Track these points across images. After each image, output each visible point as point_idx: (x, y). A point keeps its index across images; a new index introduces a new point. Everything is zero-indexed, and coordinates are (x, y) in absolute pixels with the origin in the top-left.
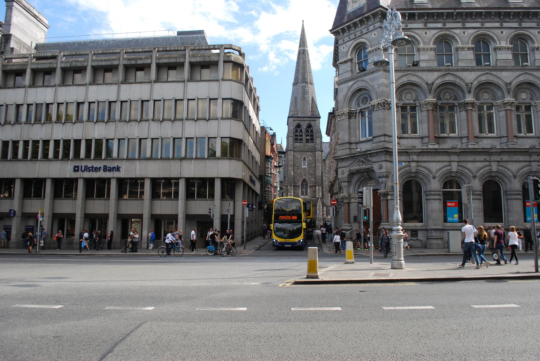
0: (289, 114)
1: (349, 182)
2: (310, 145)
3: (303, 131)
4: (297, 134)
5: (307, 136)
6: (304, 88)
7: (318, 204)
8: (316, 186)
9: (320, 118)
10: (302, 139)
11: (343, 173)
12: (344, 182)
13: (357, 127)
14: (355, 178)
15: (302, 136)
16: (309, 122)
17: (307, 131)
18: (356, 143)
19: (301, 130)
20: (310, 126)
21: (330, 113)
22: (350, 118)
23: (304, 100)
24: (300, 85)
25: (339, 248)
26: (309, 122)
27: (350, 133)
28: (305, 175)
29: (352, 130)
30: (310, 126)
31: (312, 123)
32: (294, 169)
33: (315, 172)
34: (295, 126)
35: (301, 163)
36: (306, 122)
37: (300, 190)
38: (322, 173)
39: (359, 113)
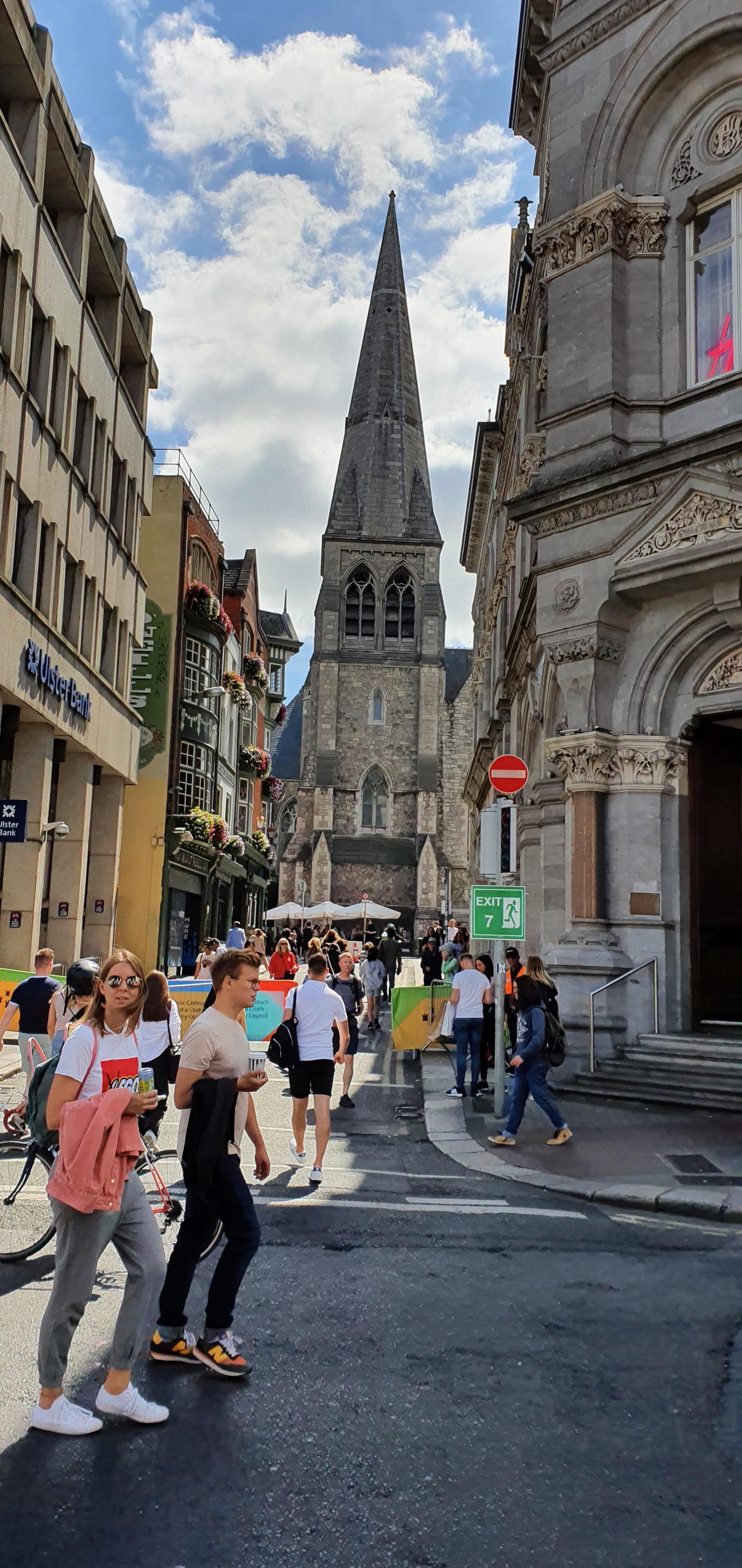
0: (330, 526)
1: (608, 655)
2: (401, 644)
3: (379, 590)
4: (355, 602)
5: (391, 609)
6: (384, 434)
7: (423, 860)
8: (415, 794)
9: (440, 545)
10: (371, 622)
11: (569, 602)
12: (575, 657)
13: (671, 307)
14: (655, 625)
15: (370, 609)
16: (397, 559)
17: (393, 592)
18: (663, 409)
19: (369, 589)
20: (401, 575)
21: (484, 428)
22: (621, 250)
23: (384, 477)
24: (372, 423)
25: (199, 848)
26: (397, 559)
27: (620, 346)
28: (378, 752)
29: (635, 330)
30: (401, 575)
31: (411, 564)
32: (339, 731)
33: (416, 743)
34: (346, 574)
35: (364, 708)
36: (388, 558)
37: (359, 808)
38: (440, 749)
39: (683, 221)
